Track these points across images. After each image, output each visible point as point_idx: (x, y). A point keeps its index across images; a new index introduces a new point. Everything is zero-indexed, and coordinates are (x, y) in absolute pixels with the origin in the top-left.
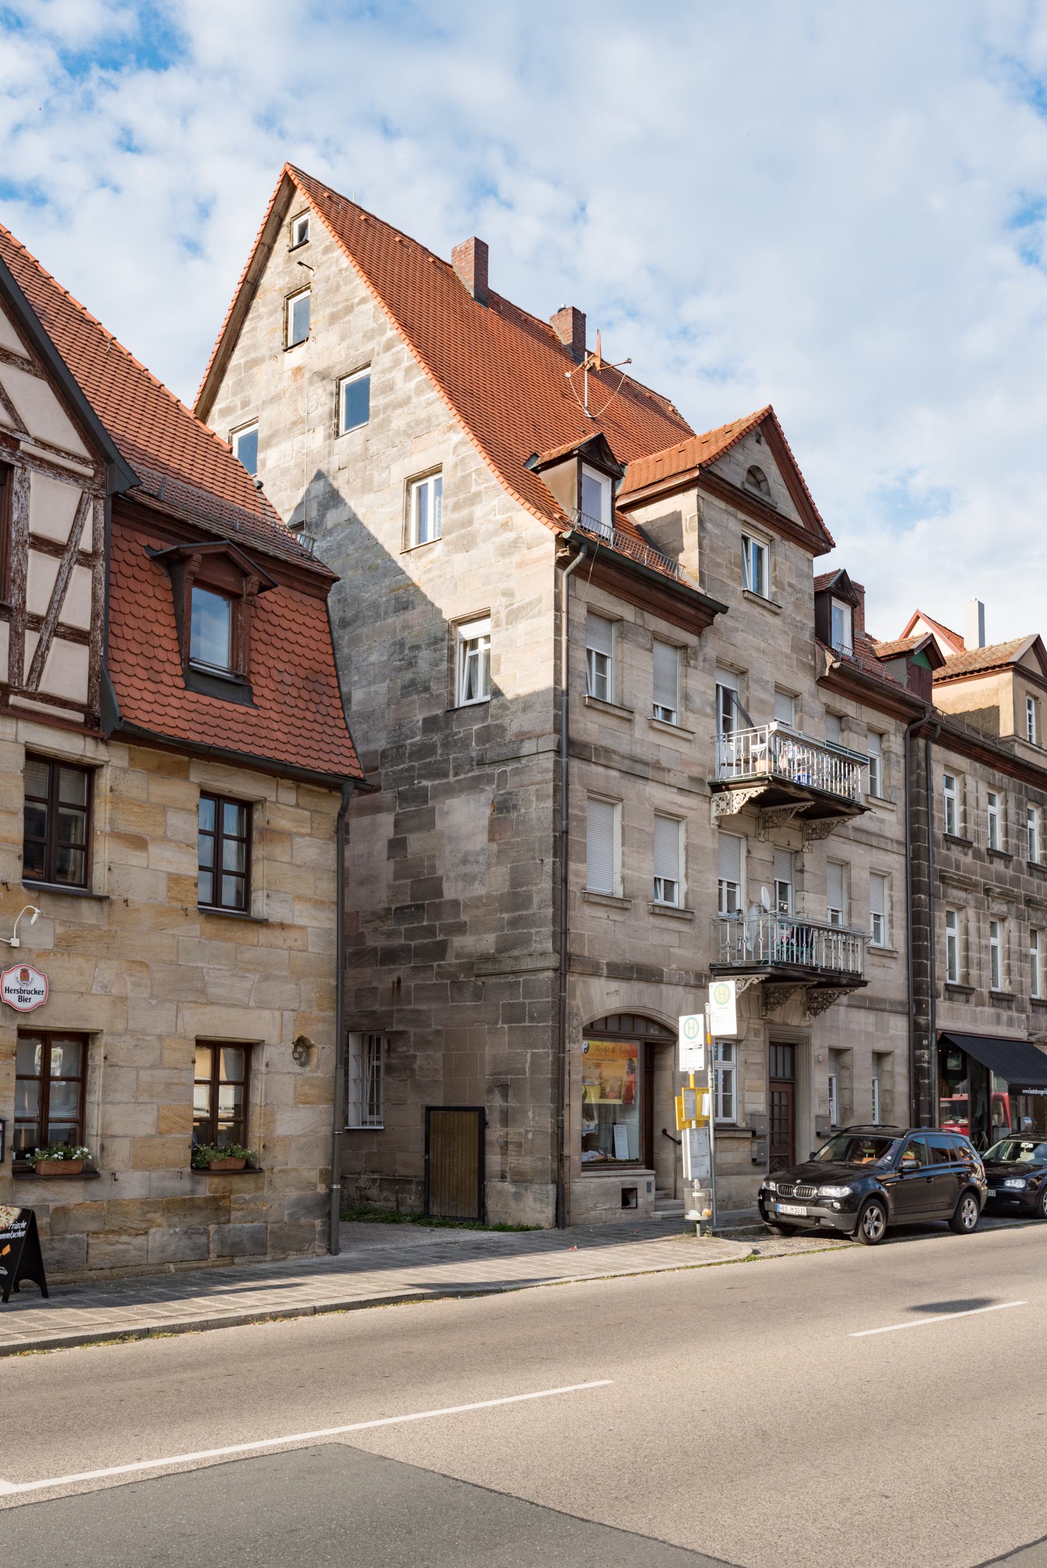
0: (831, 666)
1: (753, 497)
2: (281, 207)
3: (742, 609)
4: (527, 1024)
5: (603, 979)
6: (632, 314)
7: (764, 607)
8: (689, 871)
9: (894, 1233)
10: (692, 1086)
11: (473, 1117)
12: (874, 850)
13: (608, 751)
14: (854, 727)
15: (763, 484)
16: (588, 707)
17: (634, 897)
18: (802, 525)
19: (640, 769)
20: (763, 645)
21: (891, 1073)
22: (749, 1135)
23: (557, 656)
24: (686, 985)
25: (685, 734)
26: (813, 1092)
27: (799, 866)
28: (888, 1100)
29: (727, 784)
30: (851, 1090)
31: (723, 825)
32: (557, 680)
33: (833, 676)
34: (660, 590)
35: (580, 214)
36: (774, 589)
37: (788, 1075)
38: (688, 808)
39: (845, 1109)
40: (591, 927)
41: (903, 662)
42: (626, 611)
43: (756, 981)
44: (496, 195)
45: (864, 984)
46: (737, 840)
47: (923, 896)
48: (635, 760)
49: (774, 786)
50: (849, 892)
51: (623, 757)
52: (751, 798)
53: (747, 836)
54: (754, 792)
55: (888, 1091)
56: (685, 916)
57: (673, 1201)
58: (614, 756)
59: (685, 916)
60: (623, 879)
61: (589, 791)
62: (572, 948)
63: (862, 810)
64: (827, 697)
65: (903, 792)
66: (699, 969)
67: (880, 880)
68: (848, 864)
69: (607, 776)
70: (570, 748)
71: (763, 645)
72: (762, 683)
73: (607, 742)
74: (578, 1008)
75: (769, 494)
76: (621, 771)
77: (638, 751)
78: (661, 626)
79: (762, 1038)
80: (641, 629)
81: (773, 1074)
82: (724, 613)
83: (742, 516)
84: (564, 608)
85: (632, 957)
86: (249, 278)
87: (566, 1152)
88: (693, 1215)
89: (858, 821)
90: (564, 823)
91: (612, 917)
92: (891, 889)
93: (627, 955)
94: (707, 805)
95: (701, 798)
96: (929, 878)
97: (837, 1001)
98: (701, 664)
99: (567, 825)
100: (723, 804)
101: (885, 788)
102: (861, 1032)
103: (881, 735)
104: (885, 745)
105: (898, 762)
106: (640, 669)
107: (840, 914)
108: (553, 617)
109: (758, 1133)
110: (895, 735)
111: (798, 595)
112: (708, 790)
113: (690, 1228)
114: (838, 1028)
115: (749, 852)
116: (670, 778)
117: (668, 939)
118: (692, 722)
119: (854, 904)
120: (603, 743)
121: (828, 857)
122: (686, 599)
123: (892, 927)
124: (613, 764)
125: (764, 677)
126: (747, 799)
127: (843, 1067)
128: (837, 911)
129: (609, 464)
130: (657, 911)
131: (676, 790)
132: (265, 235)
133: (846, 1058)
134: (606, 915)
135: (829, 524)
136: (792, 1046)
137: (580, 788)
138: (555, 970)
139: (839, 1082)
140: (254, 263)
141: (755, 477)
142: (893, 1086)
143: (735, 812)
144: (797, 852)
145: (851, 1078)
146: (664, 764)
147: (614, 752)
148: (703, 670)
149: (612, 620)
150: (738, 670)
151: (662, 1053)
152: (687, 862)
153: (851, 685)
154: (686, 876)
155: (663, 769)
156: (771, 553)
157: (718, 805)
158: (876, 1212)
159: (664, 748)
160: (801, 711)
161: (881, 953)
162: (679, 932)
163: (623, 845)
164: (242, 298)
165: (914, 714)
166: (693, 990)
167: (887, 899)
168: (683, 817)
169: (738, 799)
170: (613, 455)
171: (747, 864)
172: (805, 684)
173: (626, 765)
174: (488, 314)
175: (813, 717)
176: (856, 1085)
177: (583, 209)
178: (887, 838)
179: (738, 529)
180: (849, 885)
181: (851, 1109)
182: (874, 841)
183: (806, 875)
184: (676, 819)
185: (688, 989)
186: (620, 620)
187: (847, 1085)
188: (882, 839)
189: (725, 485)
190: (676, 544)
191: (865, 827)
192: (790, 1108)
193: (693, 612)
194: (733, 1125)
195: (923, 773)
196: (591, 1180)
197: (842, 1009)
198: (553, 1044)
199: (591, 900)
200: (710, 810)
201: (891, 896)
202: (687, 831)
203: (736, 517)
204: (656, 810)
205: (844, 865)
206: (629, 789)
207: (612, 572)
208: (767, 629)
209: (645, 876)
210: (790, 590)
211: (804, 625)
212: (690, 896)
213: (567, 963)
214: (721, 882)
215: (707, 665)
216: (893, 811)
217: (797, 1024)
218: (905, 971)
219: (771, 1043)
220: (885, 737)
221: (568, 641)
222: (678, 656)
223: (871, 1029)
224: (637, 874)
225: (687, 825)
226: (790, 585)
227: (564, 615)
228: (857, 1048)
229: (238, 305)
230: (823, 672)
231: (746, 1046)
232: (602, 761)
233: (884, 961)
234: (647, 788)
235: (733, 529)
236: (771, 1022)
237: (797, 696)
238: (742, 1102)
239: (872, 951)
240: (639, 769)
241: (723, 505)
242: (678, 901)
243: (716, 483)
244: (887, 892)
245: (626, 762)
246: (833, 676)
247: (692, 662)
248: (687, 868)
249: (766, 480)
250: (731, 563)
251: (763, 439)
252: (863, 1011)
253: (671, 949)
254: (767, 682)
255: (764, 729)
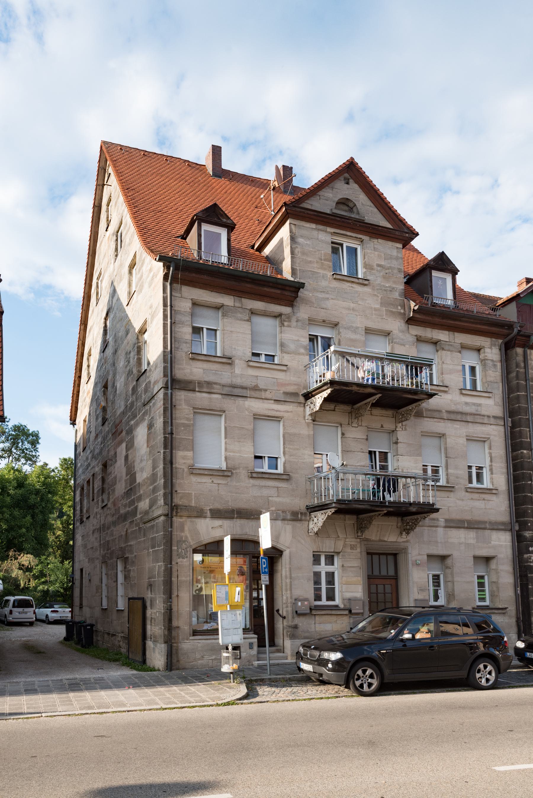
0: (414, 309)
1: (349, 218)
2: (103, 164)
3: (332, 286)
4: (157, 549)
5: (208, 520)
6: (526, 220)
7: (353, 282)
8: (286, 449)
9: (385, 689)
10: (227, 582)
11: (140, 603)
12: (470, 424)
13: (209, 384)
14: (447, 347)
15: (354, 209)
16: (193, 359)
17: (235, 469)
18: (391, 227)
19: (236, 392)
20: (352, 305)
21: (497, 571)
22: (347, 612)
23: (165, 333)
24: (283, 520)
25: (284, 368)
26: (411, 584)
27: (394, 439)
28: (495, 589)
29: (311, 392)
30: (453, 582)
31: (317, 419)
32: (165, 347)
33: (417, 316)
34: (247, 282)
35: (495, 184)
36: (365, 270)
37: (392, 572)
38: (283, 412)
39: (449, 595)
40: (191, 489)
41: (514, 305)
42: (228, 300)
43: (330, 514)
44: (450, 190)
45: (437, 510)
46: (334, 428)
47: (525, 451)
48: (234, 387)
49: (337, 387)
50: (446, 454)
51: (223, 386)
52: (325, 398)
53: (341, 425)
54: (325, 394)
55: (494, 582)
56: (286, 477)
57: (281, 654)
58: (215, 386)
59: (286, 477)
60: (226, 458)
61: (194, 408)
62: (177, 501)
63: (431, 396)
64: (416, 331)
65: (501, 384)
66: (296, 509)
67: (482, 444)
68: (444, 435)
69: (210, 398)
70: (174, 383)
71: (352, 305)
72: (355, 330)
73: (211, 378)
74: (186, 537)
75: (358, 213)
76: (222, 394)
77: (238, 381)
78: (258, 305)
79: (359, 550)
80: (240, 310)
81: (370, 574)
82: (303, 288)
83: (329, 229)
84: (169, 304)
85: (233, 505)
86: (96, 204)
87: (175, 623)
88: (226, 668)
89: (433, 402)
90: (170, 428)
91: (215, 481)
92: (490, 448)
93: (230, 504)
94: (302, 409)
95: (296, 404)
96: (530, 439)
97: (420, 523)
98: (294, 323)
99: (172, 429)
100: (312, 406)
101: (483, 384)
102: (460, 544)
103: (479, 350)
104: (482, 356)
105: (495, 366)
106: (236, 332)
107: (440, 469)
108: (162, 311)
109: (353, 611)
110: (491, 348)
111: (387, 271)
112: (302, 399)
113: (225, 676)
114: (437, 542)
115: (343, 434)
116: (268, 395)
117: (265, 492)
118: (287, 359)
119: (449, 460)
120: (207, 379)
121: (422, 432)
122: (271, 284)
123: (492, 473)
124: (213, 391)
125: (354, 325)
126: (323, 399)
127: (447, 567)
128: (426, 466)
129: (225, 220)
130: (254, 475)
131: (273, 402)
132: (99, 180)
133: (449, 561)
134: (211, 481)
135: (410, 221)
136: (395, 555)
137: (187, 407)
138: (166, 515)
139: (445, 577)
140: (97, 196)
141: (348, 206)
142: (498, 578)
143: (318, 409)
144: (393, 431)
145: (452, 574)
146: (261, 387)
147: (216, 383)
148: (296, 327)
149: (218, 308)
150: (330, 324)
151: (277, 562)
152: (284, 444)
153: (437, 320)
154: (284, 453)
155: (261, 390)
156: (362, 249)
157: (310, 407)
158: (369, 672)
159: (264, 377)
160: (392, 342)
161: (211, 473)
162: (278, 487)
163: (226, 438)
164: (95, 215)
165: (506, 331)
166: (290, 522)
167: (487, 456)
168: (281, 418)
169: (319, 400)
170: (226, 214)
171: (342, 442)
172: (396, 325)
173: (226, 390)
174: (223, 181)
175: (404, 345)
176: (456, 579)
177: (496, 181)
178: (484, 416)
179: (328, 238)
180: (446, 449)
181: (453, 595)
182: (469, 418)
183: (399, 445)
184: (277, 419)
185: (286, 522)
186: (223, 306)
187: (450, 579)
188: (476, 417)
189: (309, 212)
190: (281, 258)
191: (461, 410)
192: (394, 594)
193: (278, 291)
194: (337, 606)
195: (522, 370)
196: (200, 641)
197: (440, 531)
198: (164, 559)
199: (194, 472)
200: (304, 411)
201: (490, 454)
202: (284, 425)
203: (326, 231)
204: (254, 415)
205: (441, 436)
206: (229, 404)
207: (205, 277)
208: (357, 295)
209: (246, 456)
210: (379, 268)
211: (394, 288)
212: (286, 465)
213: (173, 510)
214: (470, 467)
215: (299, 324)
216: (489, 397)
217: (394, 540)
218: (506, 502)
219: (368, 553)
220: (482, 351)
221: (171, 322)
222: (277, 322)
223: (472, 541)
224: (238, 455)
225: (284, 422)
226: (379, 265)
227: (169, 308)
228: (456, 554)
229: (94, 218)
230: (409, 315)
231: (342, 555)
232: (205, 390)
233: (484, 496)
234: (246, 402)
235: (323, 238)
236: (367, 540)
237: (389, 334)
238: (341, 591)
239: (469, 490)
240: (237, 391)
241: (313, 226)
242: (280, 470)
243: (300, 212)
244: (487, 451)
245: (227, 389)
246: (417, 316)
247: (286, 324)
248: (284, 448)
249: (355, 205)
250: (321, 260)
251: (351, 181)
252: (462, 529)
253: (270, 498)
254: (357, 328)
255: (328, 352)
